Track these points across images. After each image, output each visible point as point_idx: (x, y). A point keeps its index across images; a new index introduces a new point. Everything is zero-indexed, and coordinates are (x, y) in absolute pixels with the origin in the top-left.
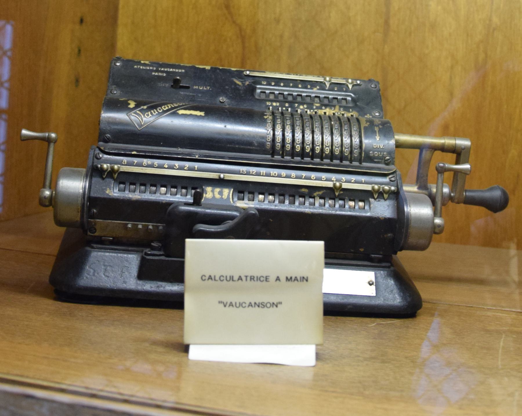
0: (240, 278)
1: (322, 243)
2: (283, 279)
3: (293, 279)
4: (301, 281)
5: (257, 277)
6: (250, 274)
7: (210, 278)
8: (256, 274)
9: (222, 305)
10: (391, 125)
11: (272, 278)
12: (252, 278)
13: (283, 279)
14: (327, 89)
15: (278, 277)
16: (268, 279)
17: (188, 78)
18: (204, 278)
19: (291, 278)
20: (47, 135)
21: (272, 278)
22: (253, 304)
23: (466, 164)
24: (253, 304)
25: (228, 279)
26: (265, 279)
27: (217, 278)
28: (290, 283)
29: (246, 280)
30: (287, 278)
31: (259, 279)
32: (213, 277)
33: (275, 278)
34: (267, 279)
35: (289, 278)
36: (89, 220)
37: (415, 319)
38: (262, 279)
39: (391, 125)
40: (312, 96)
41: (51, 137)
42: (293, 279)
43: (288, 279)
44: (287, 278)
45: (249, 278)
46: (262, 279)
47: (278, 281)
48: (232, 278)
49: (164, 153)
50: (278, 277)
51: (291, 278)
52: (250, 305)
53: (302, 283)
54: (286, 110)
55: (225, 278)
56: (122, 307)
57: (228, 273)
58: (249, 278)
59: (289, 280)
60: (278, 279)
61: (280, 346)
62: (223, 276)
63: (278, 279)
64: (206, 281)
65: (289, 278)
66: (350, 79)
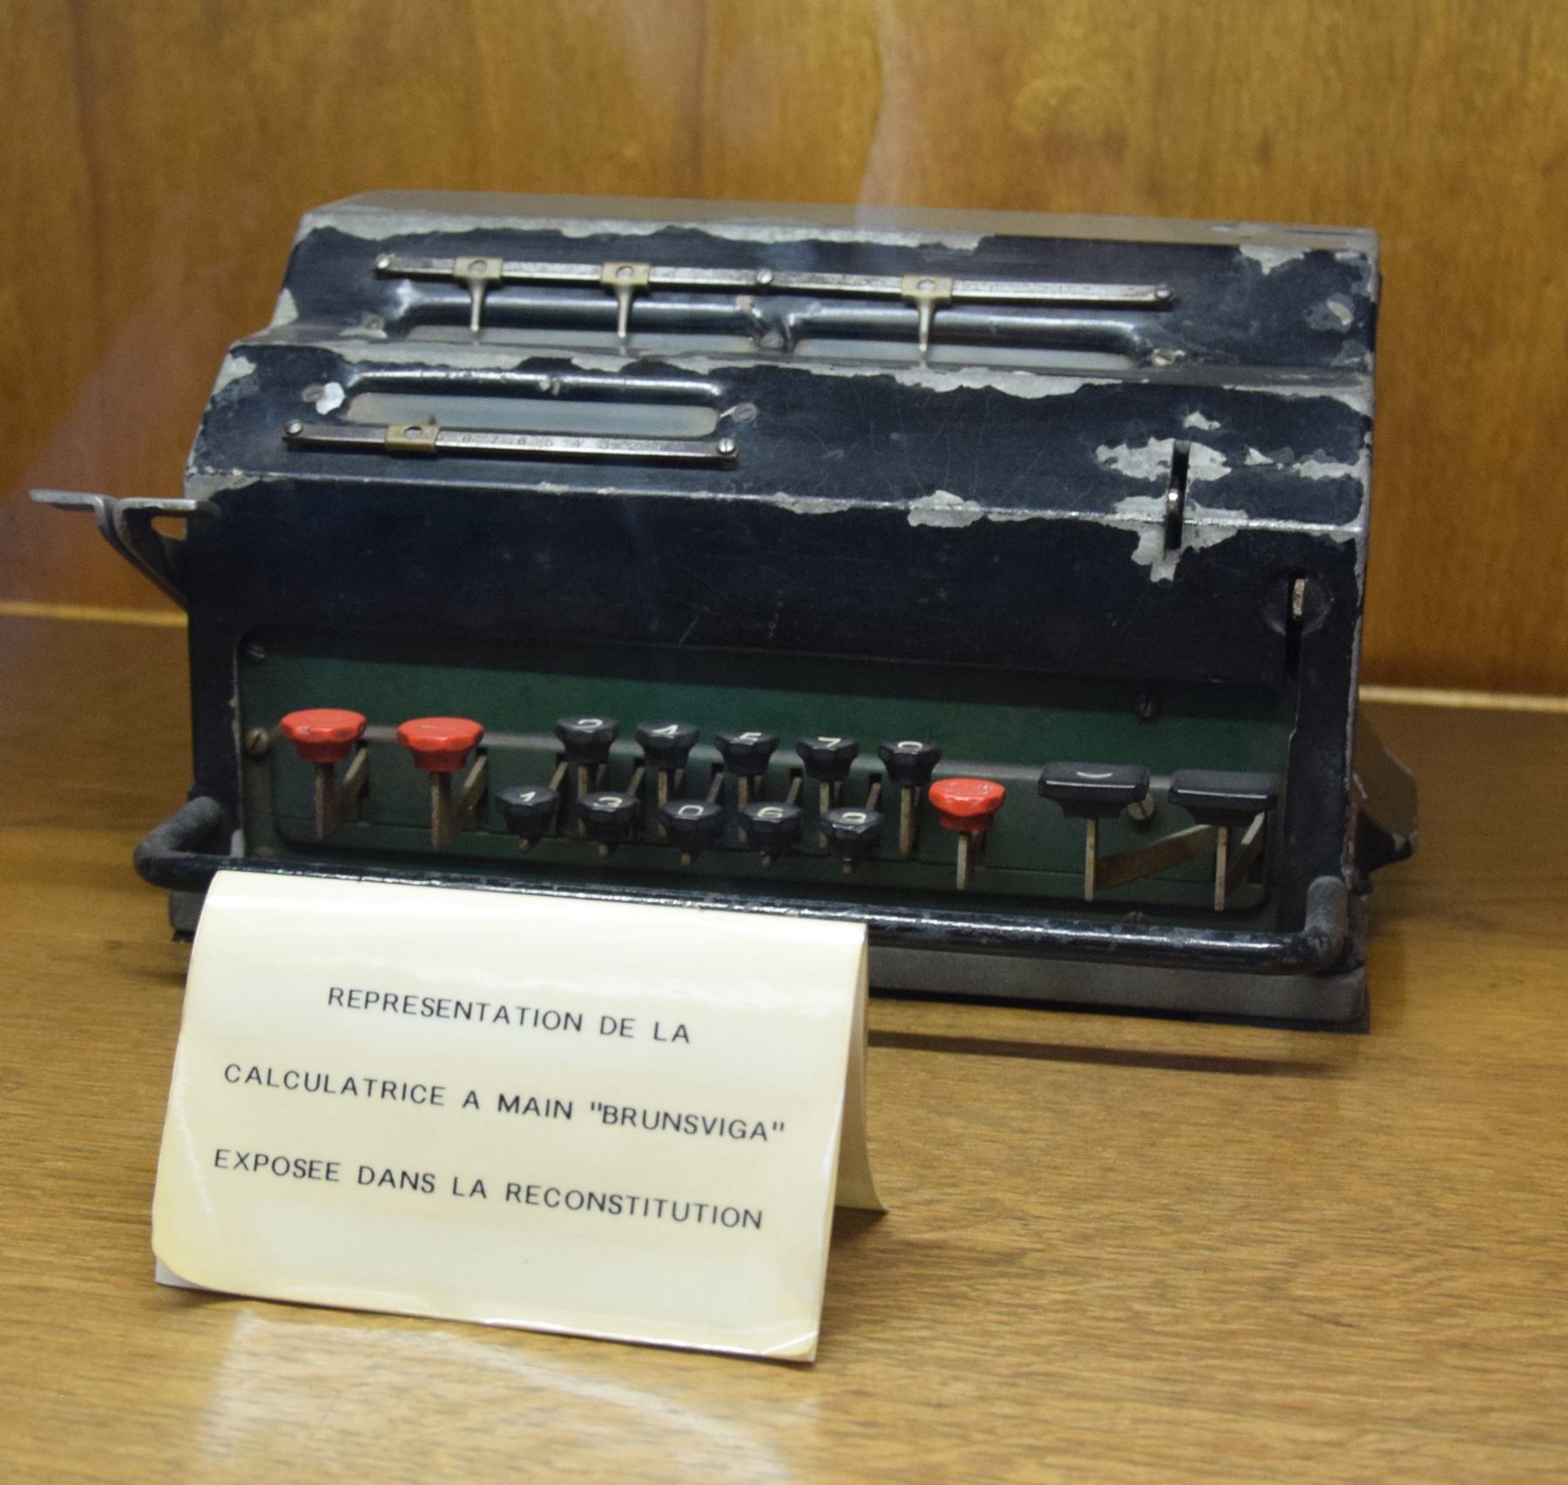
0: (350, 1085)
2: (496, 1190)
3: (523, 1104)
4: (547, 1113)
6: (381, 1076)
11: (454, 1096)
12: (388, 1089)
13: (496, 1190)
15: (479, 1182)
16: (440, 1096)
22: (397, 1178)
23: (865, 969)
24: (397, 1178)
25: (312, 1083)
26: (428, 1095)
31: (409, 1093)
35: (509, 1100)
41: (1290, 401)
42: (523, 1104)
43: (512, 1191)
48: (323, 1083)
49: (1014, 259)
50: (479, 1182)
51: (517, 1100)
55: (301, 1081)
58: (377, 1088)
60: (472, 1099)
63: (472, 1099)
65: (509, 1100)
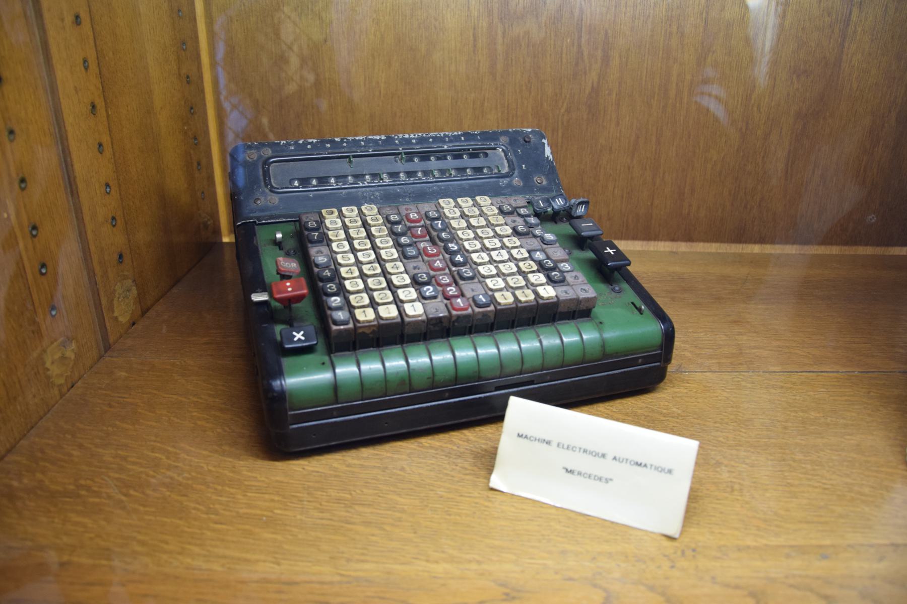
5: (590, 451)
6: (584, 447)
8: (590, 448)
10: (523, 219)
19: (522, 435)
20: (226, 240)
28: (520, 439)
29: (580, 451)
30: (518, 434)
33: (613, 457)
34: (548, 443)
35: (520, 434)
36: (540, 201)
39: (523, 219)
44: (518, 434)
45: (653, 467)
46: (532, 439)
51: (522, 435)
53: (542, 444)
56: (427, 438)
58: (582, 451)
59: (520, 436)
61: (426, 441)
62: (576, 447)
65: (520, 434)
66: (304, 331)
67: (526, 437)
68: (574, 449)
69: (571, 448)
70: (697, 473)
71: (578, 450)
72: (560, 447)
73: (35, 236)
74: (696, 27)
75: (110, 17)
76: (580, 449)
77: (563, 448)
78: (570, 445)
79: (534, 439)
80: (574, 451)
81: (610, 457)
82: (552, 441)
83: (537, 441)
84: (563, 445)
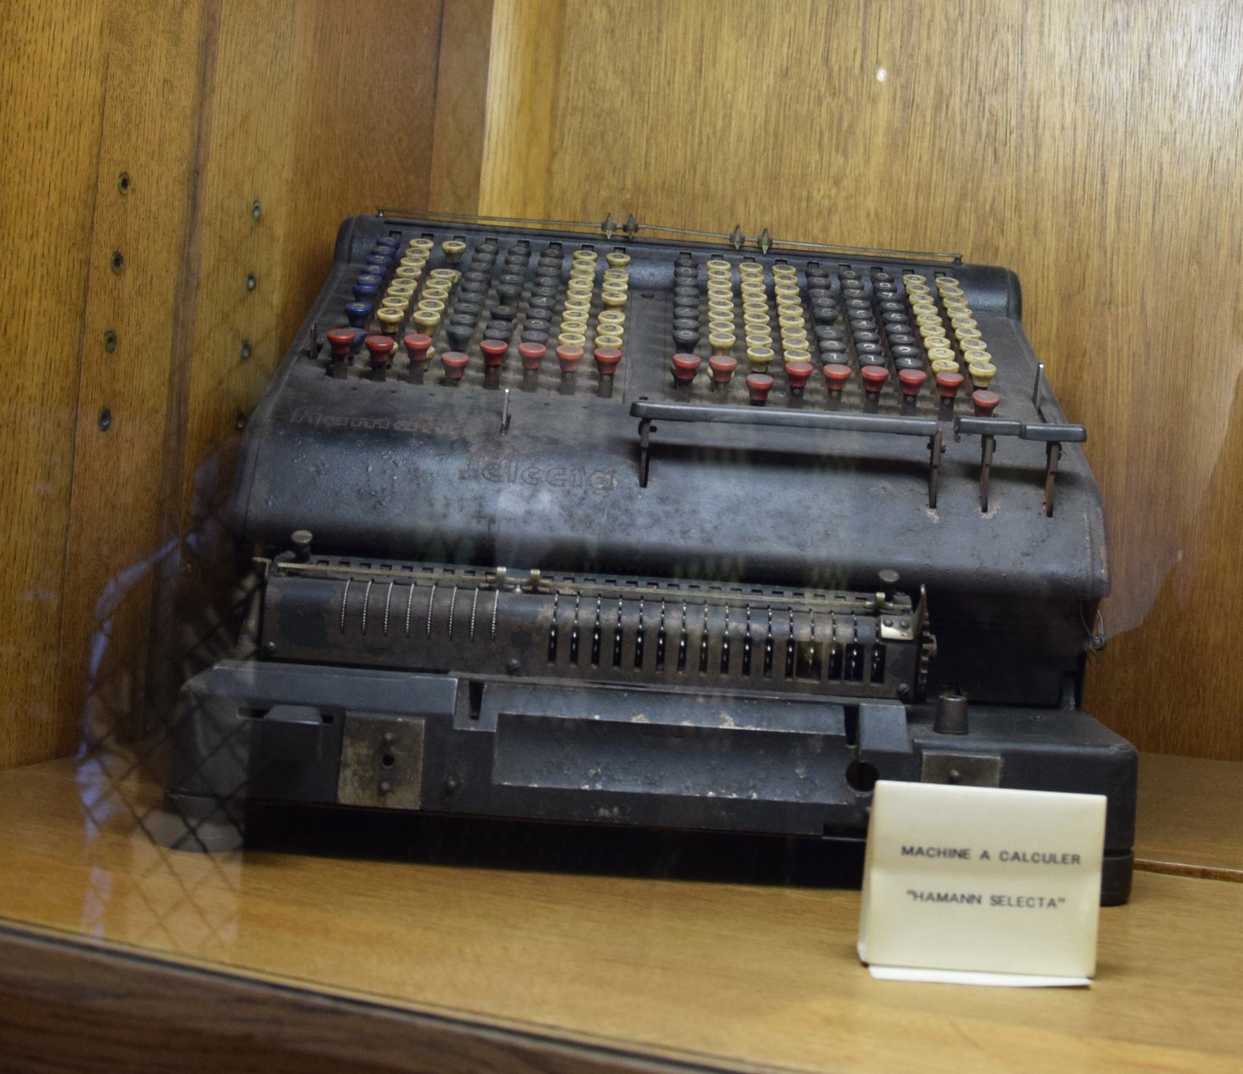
1: (1099, 801)
7: (1016, 856)
9: (911, 897)
11: (975, 853)
14: (780, 357)
17: (782, 169)
18: (1005, 856)
21: (975, 853)
27: (1028, 857)
30: (979, 901)
32: (1021, 856)
33: (980, 852)
34: (963, 854)
37: (1124, 907)
38: (931, 852)
40: (896, 402)
44: (979, 901)
47: (985, 859)
52: (930, 897)
54: (940, 446)
55: (1041, 858)
57: (1047, 850)
59: (908, 853)
60: (985, 855)
63: (985, 855)
64: (1009, 862)
67: (920, 851)
68: (1031, 903)
69: (1024, 901)
70: (203, 653)
71: (1037, 902)
72: (1003, 905)
73: (251, 277)
74: (1175, 97)
75: (1174, 101)
76: (1041, 899)
77: (1010, 904)
78: (1068, 855)
79: (935, 853)
80: (1031, 906)
81: (986, 900)
82: (969, 850)
83: (942, 856)
84: (1009, 899)
